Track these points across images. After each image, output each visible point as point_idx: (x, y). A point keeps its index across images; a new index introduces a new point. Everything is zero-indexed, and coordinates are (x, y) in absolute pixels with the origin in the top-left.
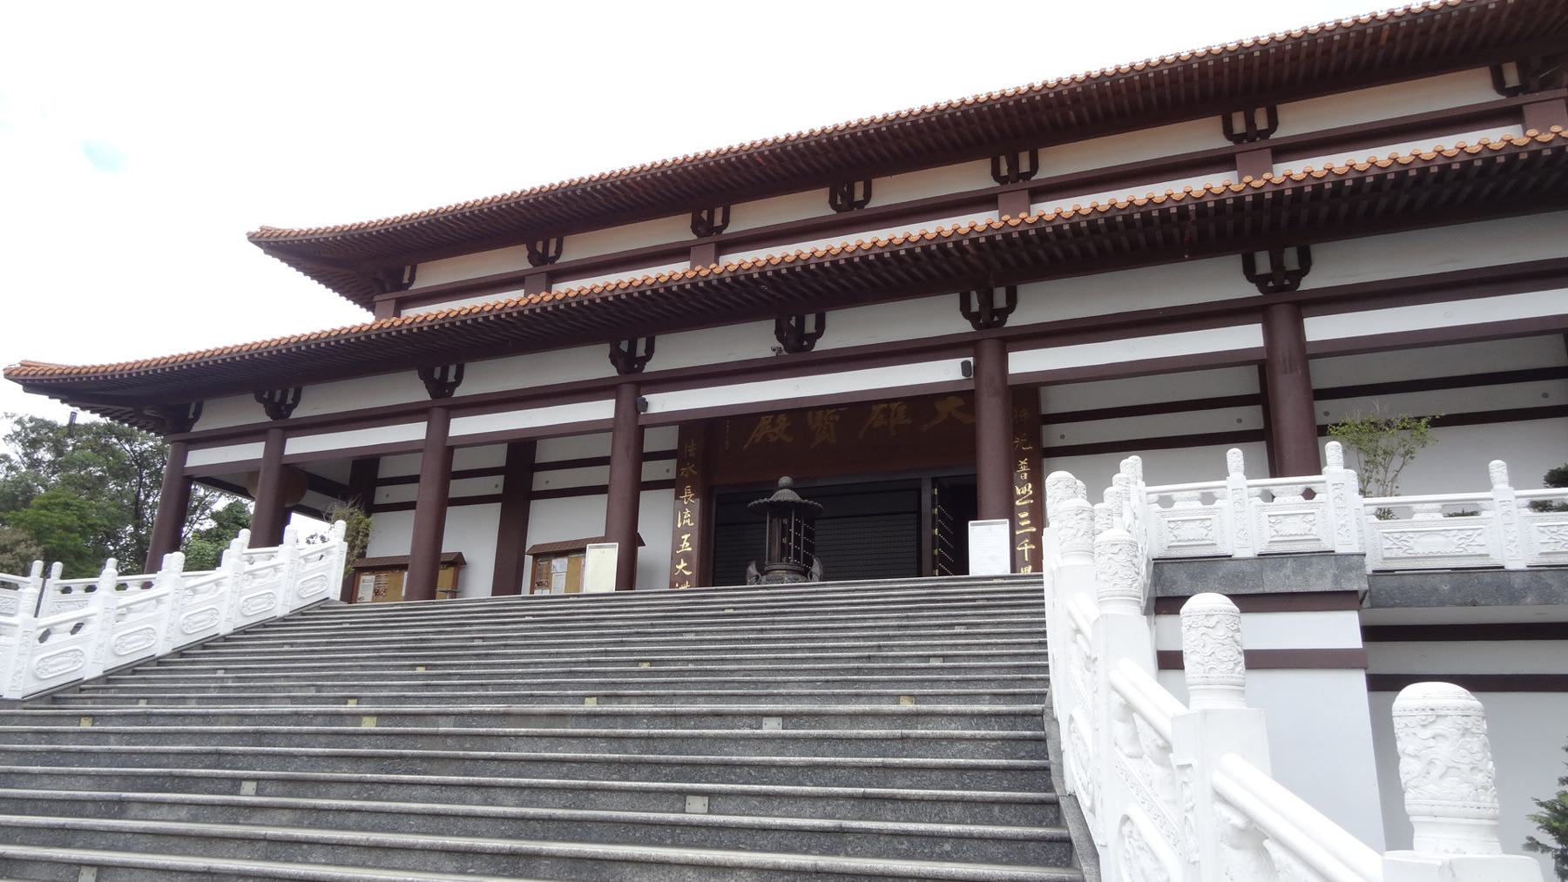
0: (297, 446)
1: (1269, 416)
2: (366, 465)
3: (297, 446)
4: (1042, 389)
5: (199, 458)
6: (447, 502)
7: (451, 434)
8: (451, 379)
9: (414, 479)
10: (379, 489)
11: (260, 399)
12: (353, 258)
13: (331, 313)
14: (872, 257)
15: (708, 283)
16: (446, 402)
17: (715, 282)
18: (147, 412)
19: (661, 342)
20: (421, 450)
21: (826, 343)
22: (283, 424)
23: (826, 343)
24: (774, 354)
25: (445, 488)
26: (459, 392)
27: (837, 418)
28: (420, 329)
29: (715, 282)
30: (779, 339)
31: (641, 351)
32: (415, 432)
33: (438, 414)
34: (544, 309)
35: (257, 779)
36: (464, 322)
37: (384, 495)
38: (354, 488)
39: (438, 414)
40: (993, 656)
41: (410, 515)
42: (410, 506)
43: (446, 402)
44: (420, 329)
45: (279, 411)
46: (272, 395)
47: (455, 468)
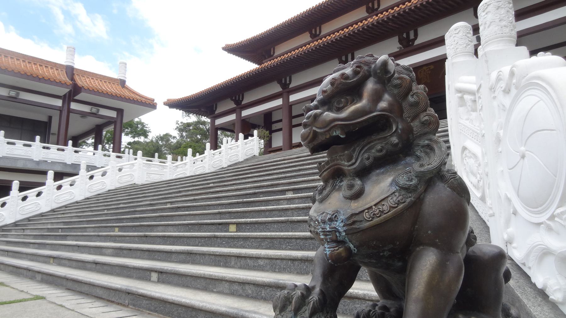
0: (245, 113)
1: (291, 122)
2: (268, 115)
3: (245, 113)
4: (274, 113)
5: (219, 122)
6: (292, 126)
7: (290, 100)
8: (288, 82)
9: (281, 121)
10: (273, 125)
11: (232, 100)
12: (242, 50)
13: (244, 67)
14: (419, 6)
15: (349, 34)
16: (287, 90)
17: (371, 26)
18: (202, 110)
19: (421, 30)
20: (281, 108)
21: (419, 41)
22: (287, 91)
23: (419, 41)
24: (398, 50)
25: (291, 122)
26: (243, 103)
27: (430, 72)
28: (274, 65)
29: (371, 26)
30: (400, 44)
31: (412, 36)
32: (278, 102)
33: (238, 110)
34: (312, 49)
35: (237, 224)
36: (287, 60)
37: (275, 127)
38: (267, 123)
39: (285, 95)
40: (234, 184)
41: (281, 132)
42: (280, 130)
43: (287, 90)
44: (274, 65)
45: (285, 86)
46: (236, 98)
47: (293, 115)
